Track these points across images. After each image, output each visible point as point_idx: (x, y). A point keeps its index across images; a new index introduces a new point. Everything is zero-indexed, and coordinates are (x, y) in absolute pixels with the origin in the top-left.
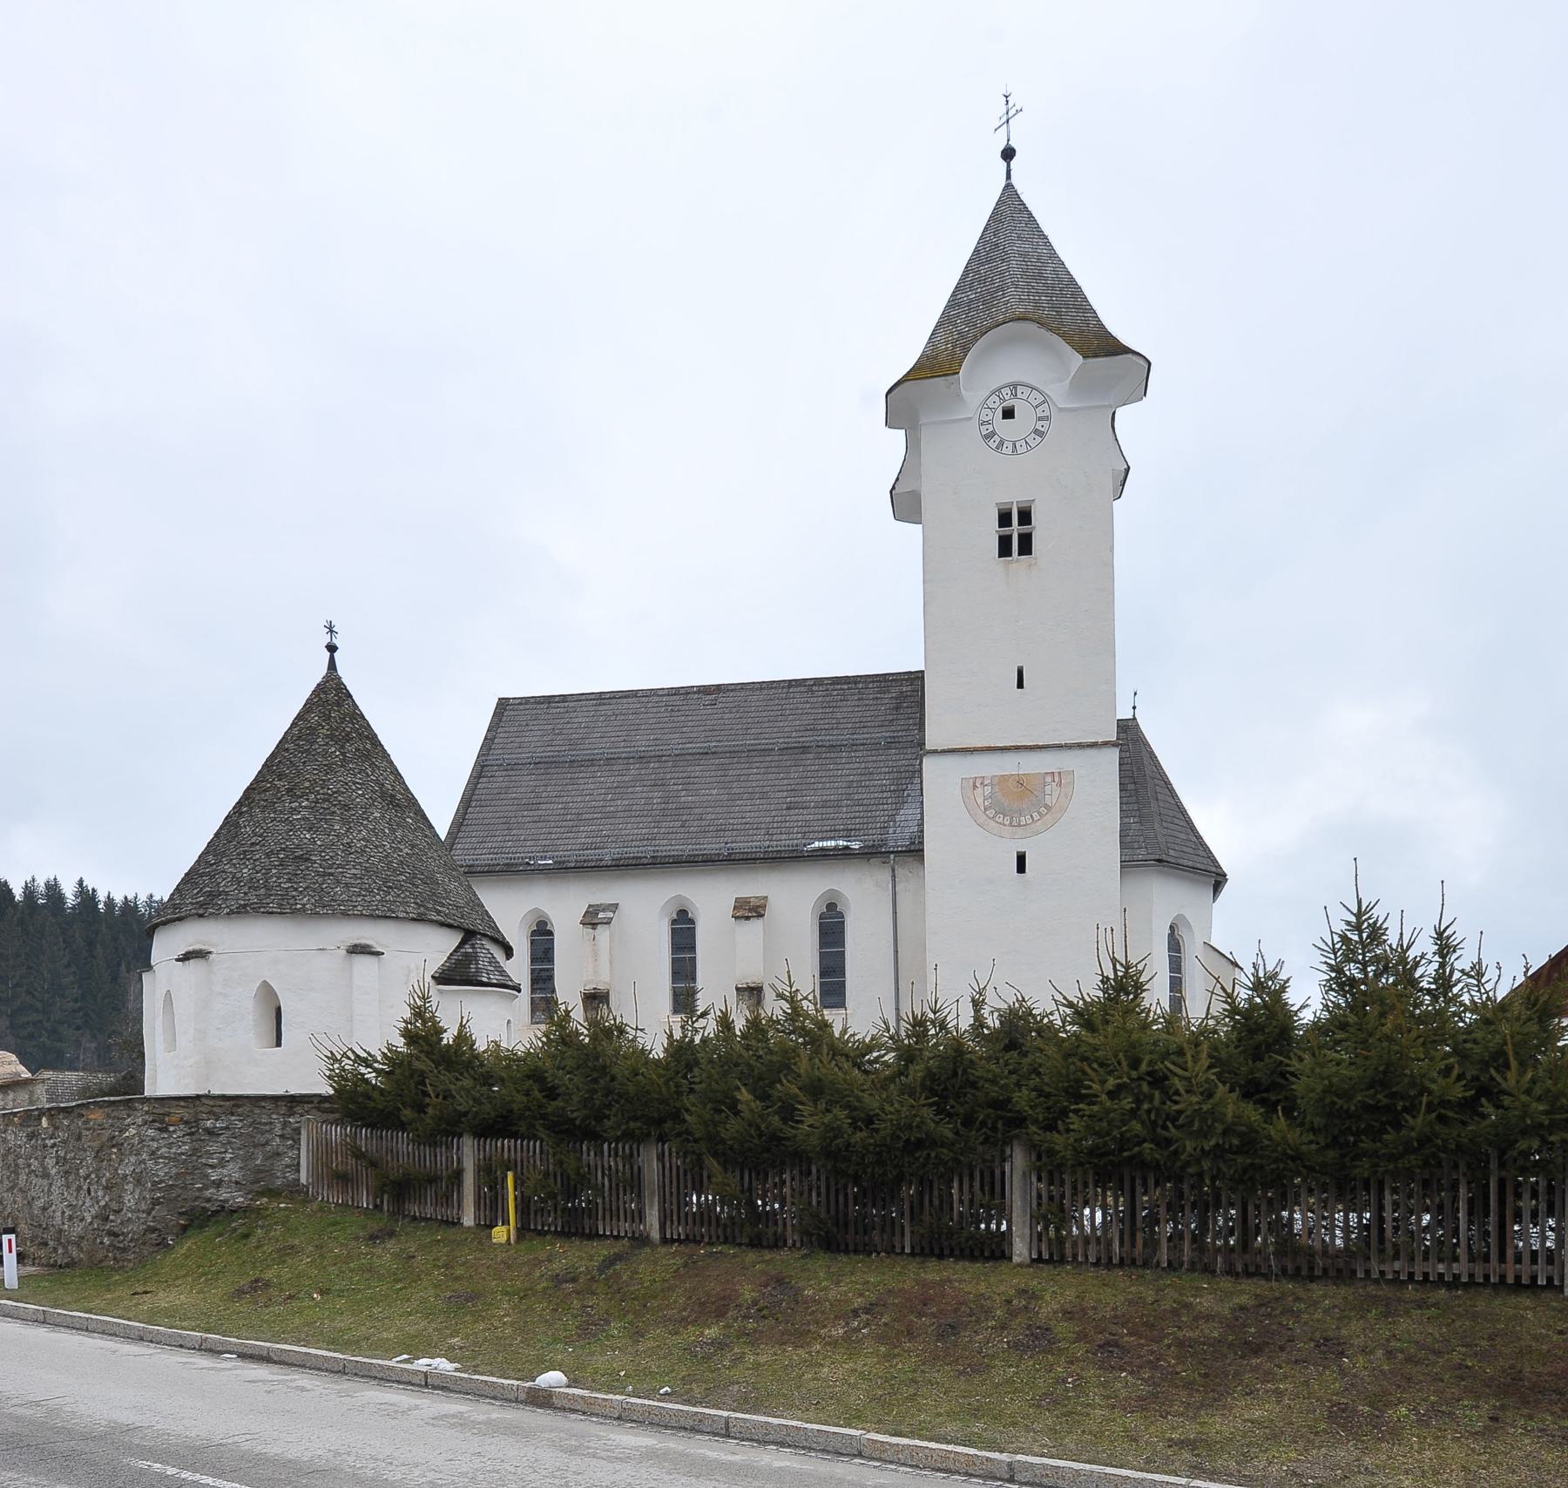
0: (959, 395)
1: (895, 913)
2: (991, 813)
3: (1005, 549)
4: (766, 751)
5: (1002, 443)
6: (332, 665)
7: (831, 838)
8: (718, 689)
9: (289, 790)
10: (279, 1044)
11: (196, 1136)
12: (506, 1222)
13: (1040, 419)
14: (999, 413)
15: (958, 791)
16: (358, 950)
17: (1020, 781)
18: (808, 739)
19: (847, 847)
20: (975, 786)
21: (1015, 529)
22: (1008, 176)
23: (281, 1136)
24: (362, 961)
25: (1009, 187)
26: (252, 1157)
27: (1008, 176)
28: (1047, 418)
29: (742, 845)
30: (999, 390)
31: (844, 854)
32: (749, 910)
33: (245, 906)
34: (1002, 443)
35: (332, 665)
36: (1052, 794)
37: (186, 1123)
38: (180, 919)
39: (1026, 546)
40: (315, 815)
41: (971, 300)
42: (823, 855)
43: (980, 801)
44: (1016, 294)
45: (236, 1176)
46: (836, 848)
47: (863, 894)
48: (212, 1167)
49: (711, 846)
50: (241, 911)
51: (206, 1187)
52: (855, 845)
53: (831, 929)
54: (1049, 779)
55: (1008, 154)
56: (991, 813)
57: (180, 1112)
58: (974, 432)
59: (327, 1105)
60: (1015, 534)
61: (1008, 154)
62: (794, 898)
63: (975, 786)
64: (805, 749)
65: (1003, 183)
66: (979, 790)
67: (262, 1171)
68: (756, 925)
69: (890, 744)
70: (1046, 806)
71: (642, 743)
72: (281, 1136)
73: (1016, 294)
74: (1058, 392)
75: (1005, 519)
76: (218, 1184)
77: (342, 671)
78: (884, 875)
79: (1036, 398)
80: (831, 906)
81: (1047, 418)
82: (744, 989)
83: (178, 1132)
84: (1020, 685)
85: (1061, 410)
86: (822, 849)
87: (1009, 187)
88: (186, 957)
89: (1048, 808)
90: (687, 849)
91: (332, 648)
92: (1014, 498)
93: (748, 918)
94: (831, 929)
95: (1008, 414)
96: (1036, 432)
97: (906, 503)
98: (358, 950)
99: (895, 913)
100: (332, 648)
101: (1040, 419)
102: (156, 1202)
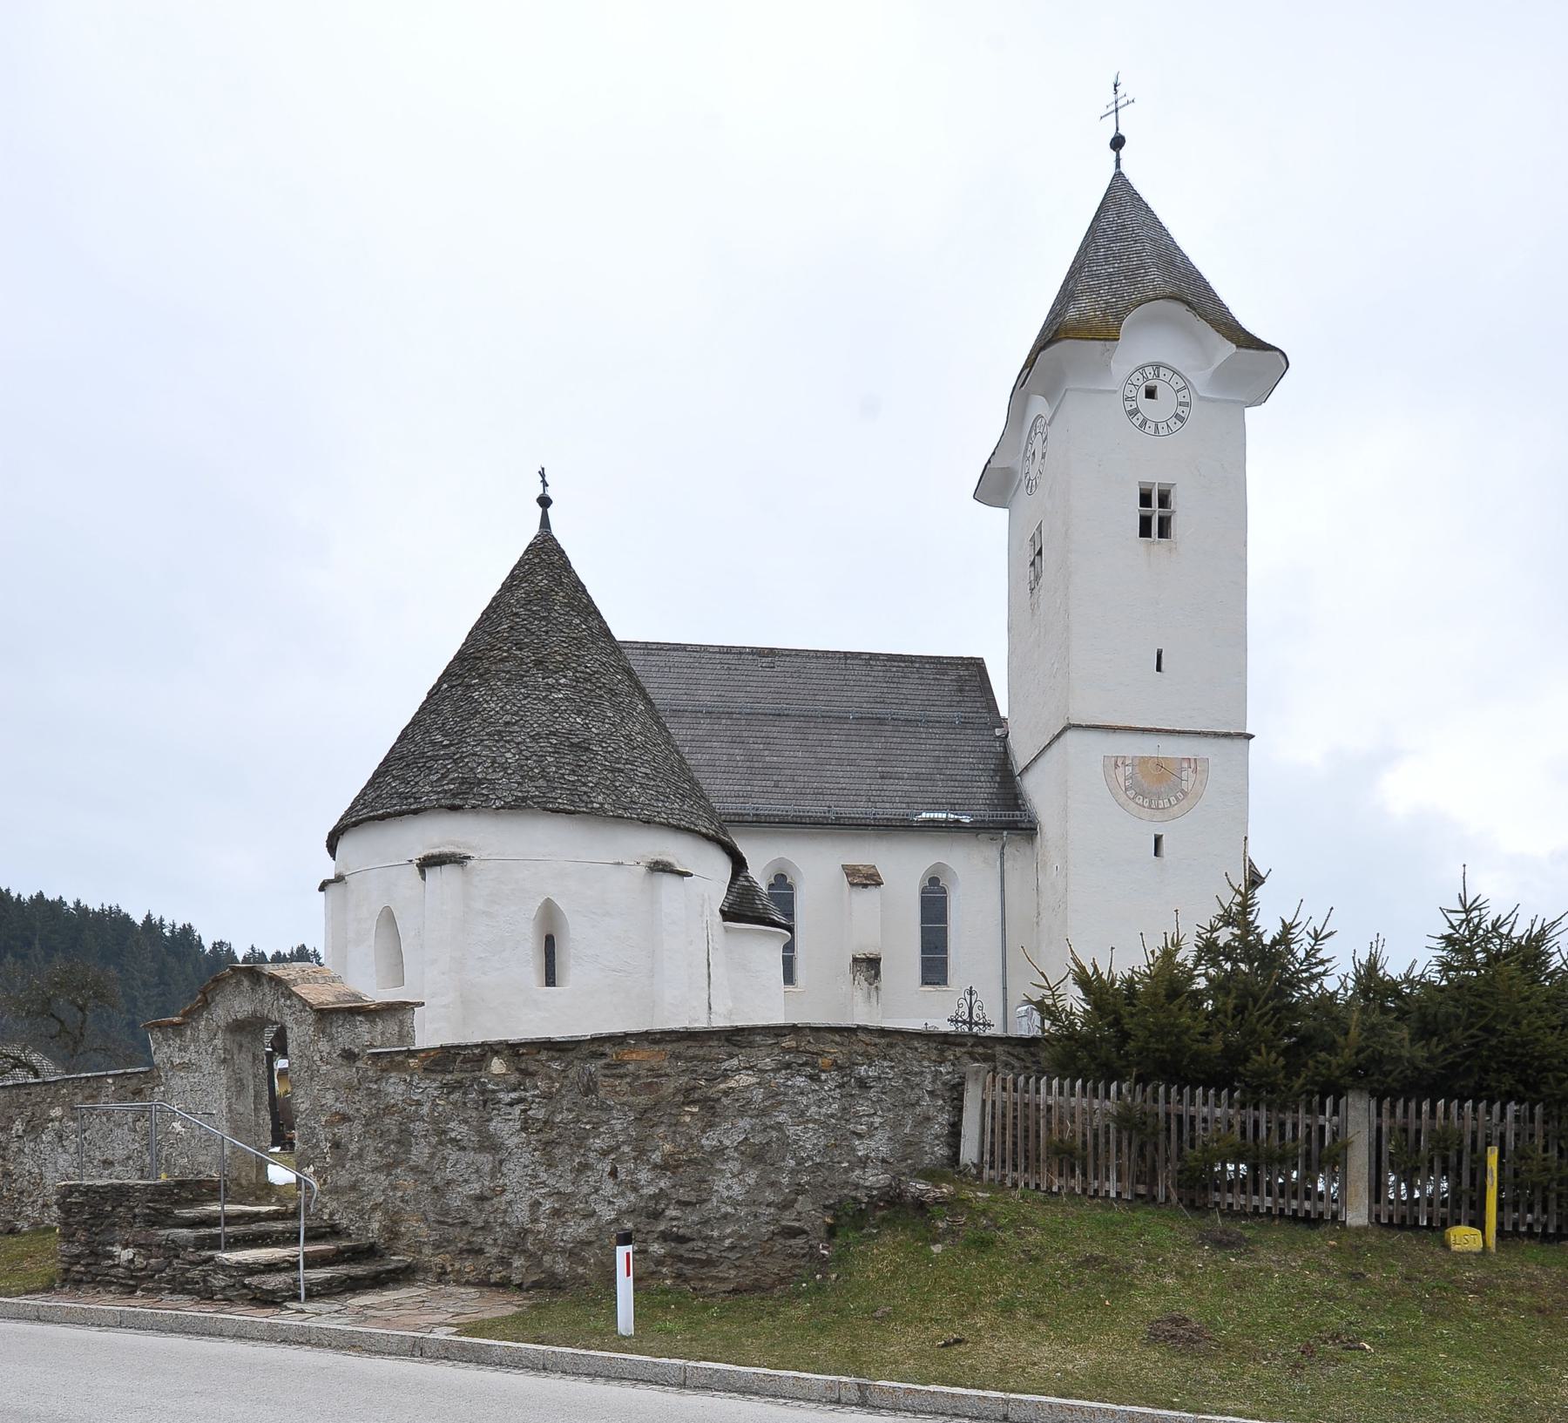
0: (1108, 365)
1: (1003, 890)
2: (1131, 793)
3: (1145, 530)
4: (842, 719)
5: (1144, 422)
6: (545, 522)
7: (939, 811)
8: (772, 652)
9: (538, 663)
10: (550, 979)
11: (847, 1089)
12: (1478, 1222)
13: (1181, 404)
14: (1142, 391)
15: (1100, 769)
16: (660, 868)
17: (1159, 764)
18: (879, 710)
19: (957, 821)
20: (1116, 765)
21: (1155, 511)
22: (1118, 166)
23: (931, 1093)
24: (668, 881)
25: (1119, 175)
26: (898, 1124)
27: (1118, 166)
28: (1186, 404)
29: (848, 810)
30: (1143, 367)
31: (955, 827)
32: (865, 879)
33: (524, 799)
34: (1144, 422)
35: (545, 522)
36: (1189, 780)
37: (840, 1068)
38: (415, 812)
39: (1164, 532)
40: (538, 704)
41: (1110, 274)
42: (933, 826)
43: (1121, 780)
44: (1126, 279)
45: (884, 1150)
46: (946, 821)
47: (971, 872)
48: (860, 1136)
49: (815, 808)
50: (518, 806)
51: (851, 1169)
52: (966, 820)
53: (934, 905)
54: (1185, 765)
55: (1118, 143)
56: (1131, 793)
57: (834, 1052)
58: (1118, 407)
59: (980, 1050)
60: (1155, 516)
61: (1118, 143)
62: (904, 866)
63: (1116, 765)
64: (881, 721)
65: (1112, 171)
66: (1121, 769)
67: (910, 1144)
68: (872, 894)
69: (965, 724)
70: (1182, 791)
71: (706, 697)
72: (931, 1093)
73: (1126, 279)
74: (1199, 379)
75: (1145, 500)
76: (863, 1162)
77: (556, 531)
78: (992, 852)
79: (1177, 382)
80: (934, 881)
81: (1186, 404)
82: (863, 960)
83: (831, 1080)
84: (1159, 669)
85: (1201, 398)
86: (933, 820)
87: (1119, 175)
88: (429, 863)
89: (1185, 794)
90: (791, 809)
91: (545, 502)
92: (1156, 478)
93: (865, 886)
94: (934, 905)
95: (1151, 393)
96: (1176, 415)
97: (995, 486)
98: (660, 868)
99: (1003, 890)
100: (545, 502)
101: (1181, 404)
102: (799, 1190)
